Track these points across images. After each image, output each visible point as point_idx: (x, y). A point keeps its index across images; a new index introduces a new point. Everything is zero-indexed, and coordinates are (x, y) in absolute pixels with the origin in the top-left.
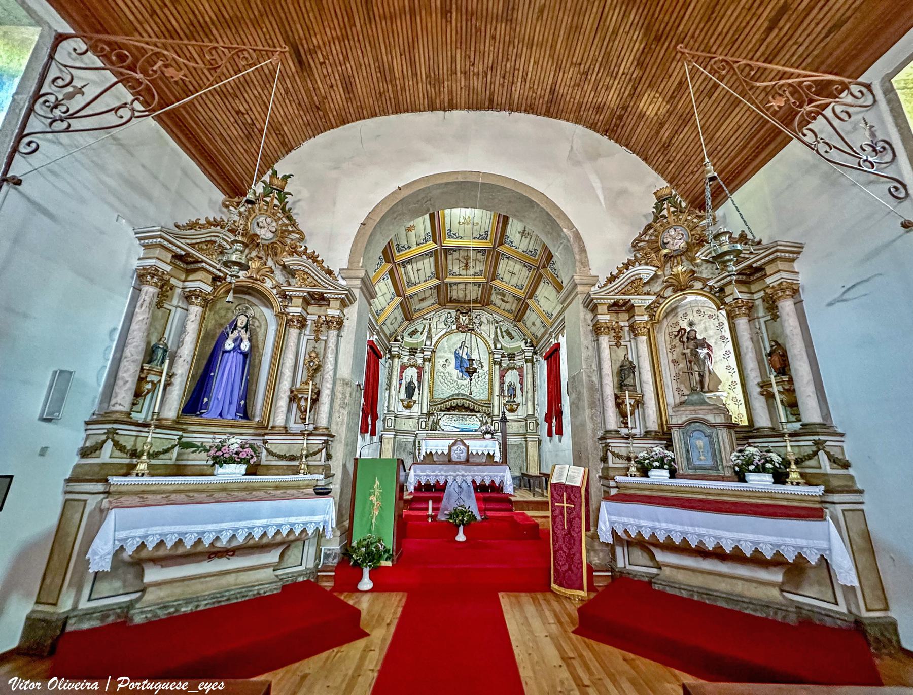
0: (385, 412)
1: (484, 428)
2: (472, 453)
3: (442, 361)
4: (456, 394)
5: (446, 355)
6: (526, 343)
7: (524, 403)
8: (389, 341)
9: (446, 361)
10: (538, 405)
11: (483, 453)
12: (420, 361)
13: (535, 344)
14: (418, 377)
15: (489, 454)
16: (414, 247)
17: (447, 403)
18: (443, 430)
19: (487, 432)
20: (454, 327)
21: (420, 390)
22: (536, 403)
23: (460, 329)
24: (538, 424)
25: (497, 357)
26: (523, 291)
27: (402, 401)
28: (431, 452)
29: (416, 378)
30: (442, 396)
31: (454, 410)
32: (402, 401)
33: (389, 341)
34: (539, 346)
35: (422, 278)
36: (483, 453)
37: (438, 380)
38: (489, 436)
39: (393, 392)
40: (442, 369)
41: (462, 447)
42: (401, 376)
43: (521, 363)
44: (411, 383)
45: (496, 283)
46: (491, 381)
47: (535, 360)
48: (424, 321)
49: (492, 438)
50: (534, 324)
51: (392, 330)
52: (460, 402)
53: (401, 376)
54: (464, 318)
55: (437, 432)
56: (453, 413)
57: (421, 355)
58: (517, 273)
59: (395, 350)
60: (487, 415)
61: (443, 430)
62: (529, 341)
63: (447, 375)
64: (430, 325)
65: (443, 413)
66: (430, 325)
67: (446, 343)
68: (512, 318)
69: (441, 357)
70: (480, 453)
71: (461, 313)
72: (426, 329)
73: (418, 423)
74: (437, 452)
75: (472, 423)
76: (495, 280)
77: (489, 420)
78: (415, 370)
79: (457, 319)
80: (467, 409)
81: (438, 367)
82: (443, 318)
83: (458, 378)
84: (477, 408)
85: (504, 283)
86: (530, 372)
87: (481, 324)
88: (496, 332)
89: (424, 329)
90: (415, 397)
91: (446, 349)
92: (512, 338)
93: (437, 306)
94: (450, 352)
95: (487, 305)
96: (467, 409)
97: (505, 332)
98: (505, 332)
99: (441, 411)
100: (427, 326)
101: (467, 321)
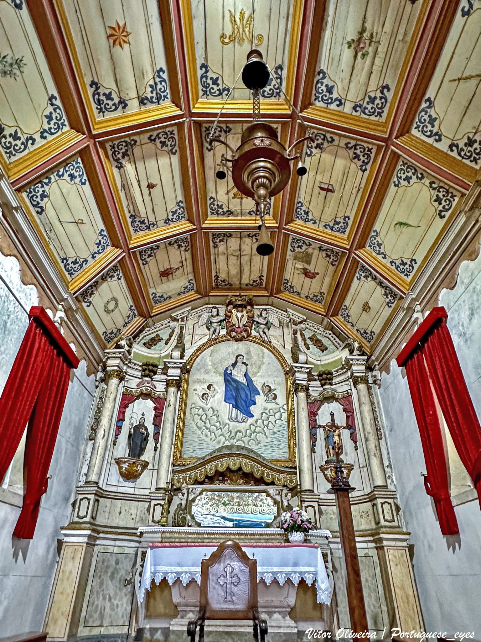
0: (81, 484)
1: (286, 516)
2: (263, 581)
3: (201, 388)
4: (227, 447)
5: (207, 377)
6: (351, 352)
7: (362, 462)
8: (104, 347)
9: (209, 387)
10: (390, 466)
11: (289, 581)
12: (160, 387)
13: (368, 351)
14: (156, 416)
15: (302, 582)
16: (134, 105)
17: (208, 467)
18: (199, 525)
19: (296, 527)
20: (223, 332)
21: (156, 443)
22: (386, 463)
23: (234, 334)
24: (398, 509)
25: (301, 377)
26: (345, 236)
27: (118, 462)
28: (164, 580)
29: (152, 419)
30: (200, 454)
31: (223, 481)
32: (118, 462)
33: (104, 347)
34: (377, 353)
35: (161, 215)
36: (289, 581)
37: (192, 424)
38: (297, 536)
39: (101, 442)
40: (201, 403)
41: (237, 565)
42: (122, 413)
43: (346, 388)
44: (141, 425)
45: (298, 225)
46: (292, 423)
47: (371, 381)
48: (173, 324)
49: (306, 541)
50: (366, 307)
51: (110, 327)
52: (233, 463)
53: (122, 413)
54: (239, 315)
55: (186, 529)
56: (222, 486)
57: (164, 377)
58: (336, 187)
59: (113, 364)
60: (291, 490)
61: (199, 525)
62: (356, 345)
63: (210, 413)
64: (182, 328)
65: (199, 488)
66: (182, 328)
67: (208, 359)
68: (323, 311)
69: (199, 381)
70: (281, 581)
71: (236, 306)
72: (175, 337)
73: (148, 510)
74: (178, 581)
75: (259, 509)
76: (292, 221)
77: (295, 501)
78: (150, 404)
79: (228, 317)
80: (248, 477)
81: (194, 398)
82: (205, 316)
83: (230, 419)
84: (268, 475)
85: (310, 224)
86: (365, 399)
87: (268, 325)
88: (295, 340)
89: (171, 336)
90: (147, 456)
91: (210, 367)
92: (323, 348)
93: (192, 295)
94: (216, 372)
95: (279, 291)
96: (248, 477)
97: (311, 339)
98: (311, 339)
99: (196, 482)
100: (177, 331)
101: (245, 320)
